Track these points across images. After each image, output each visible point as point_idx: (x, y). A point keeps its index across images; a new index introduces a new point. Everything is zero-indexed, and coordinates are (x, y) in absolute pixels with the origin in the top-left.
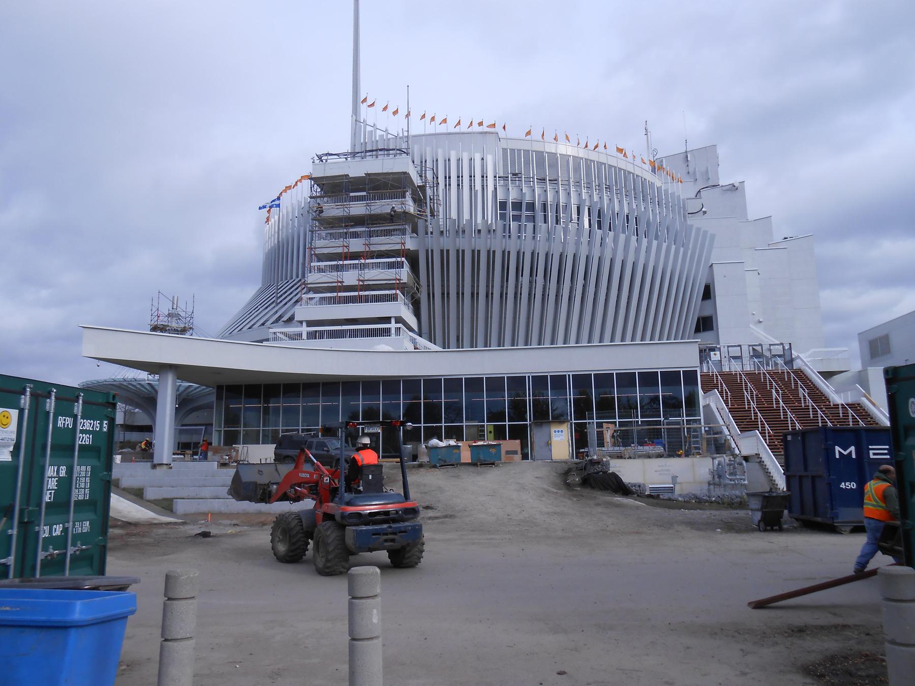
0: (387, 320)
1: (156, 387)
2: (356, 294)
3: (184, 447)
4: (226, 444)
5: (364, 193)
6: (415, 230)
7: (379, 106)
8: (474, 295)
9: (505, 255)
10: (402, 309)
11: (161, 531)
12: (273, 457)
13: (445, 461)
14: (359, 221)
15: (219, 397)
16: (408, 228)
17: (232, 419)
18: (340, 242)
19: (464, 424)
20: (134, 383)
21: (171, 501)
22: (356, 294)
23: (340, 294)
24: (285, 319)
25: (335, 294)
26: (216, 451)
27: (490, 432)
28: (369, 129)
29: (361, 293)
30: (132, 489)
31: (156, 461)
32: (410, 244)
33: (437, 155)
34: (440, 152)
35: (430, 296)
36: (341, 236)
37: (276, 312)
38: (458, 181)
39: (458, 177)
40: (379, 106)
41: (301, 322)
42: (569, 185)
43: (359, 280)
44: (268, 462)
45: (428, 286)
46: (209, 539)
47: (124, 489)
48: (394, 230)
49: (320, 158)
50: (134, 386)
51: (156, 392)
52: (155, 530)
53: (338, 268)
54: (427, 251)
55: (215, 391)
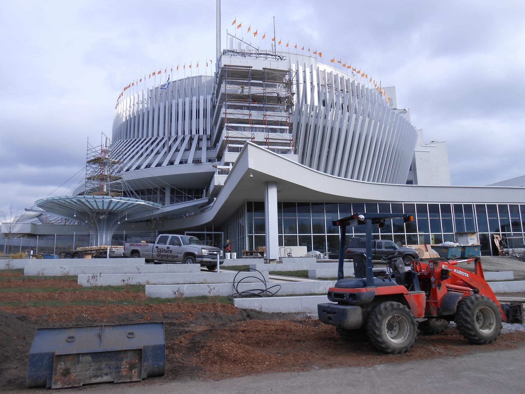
14: (255, 99)
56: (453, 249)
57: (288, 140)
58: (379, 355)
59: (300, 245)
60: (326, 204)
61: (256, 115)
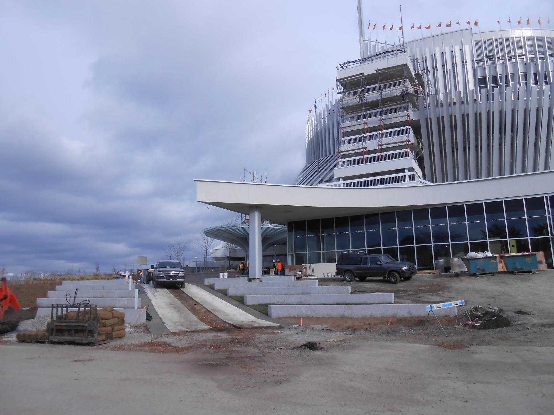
0: (403, 170)
1: (247, 230)
2: (377, 154)
3: (266, 271)
4: (297, 264)
5: (377, 85)
6: (414, 106)
7: (380, 27)
8: (466, 149)
9: (489, 115)
10: (411, 162)
11: (264, 337)
12: (336, 270)
13: (484, 270)
14: (374, 105)
15: (290, 230)
16: (410, 105)
17: (300, 246)
18: (361, 121)
19: (488, 240)
20: (234, 228)
21: (266, 305)
22: (377, 154)
23: (365, 156)
24: (326, 179)
25: (362, 157)
26: (291, 269)
27: (513, 246)
28: (373, 44)
29: (381, 154)
30: (236, 296)
31: (251, 277)
32: (413, 116)
33: (425, 53)
34: (427, 50)
35: (431, 153)
36: (361, 117)
37: (319, 177)
38: (444, 68)
39: (443, 66)
40: (380, 27)
41: (339, 179)
42: (536, 57)
43: (379, 145)
44: (330, 276)
45: (429, 145)
46: (318, 353)
47: (230, 297)
48: (398, 108)
49: (342, 66)
50: (234, 230)
51: (248, 234)
52: (257, 336)
53: (361, 140)
54: (427, 119)
55: (285, 227)
56: (478, 261)
57: (405, 142)
58: (4, 335)
59: (324, 262)
60: (382, 214)
61: (374, 121)
